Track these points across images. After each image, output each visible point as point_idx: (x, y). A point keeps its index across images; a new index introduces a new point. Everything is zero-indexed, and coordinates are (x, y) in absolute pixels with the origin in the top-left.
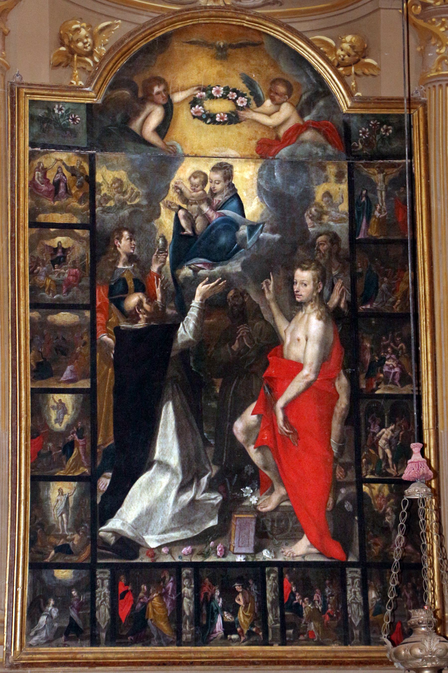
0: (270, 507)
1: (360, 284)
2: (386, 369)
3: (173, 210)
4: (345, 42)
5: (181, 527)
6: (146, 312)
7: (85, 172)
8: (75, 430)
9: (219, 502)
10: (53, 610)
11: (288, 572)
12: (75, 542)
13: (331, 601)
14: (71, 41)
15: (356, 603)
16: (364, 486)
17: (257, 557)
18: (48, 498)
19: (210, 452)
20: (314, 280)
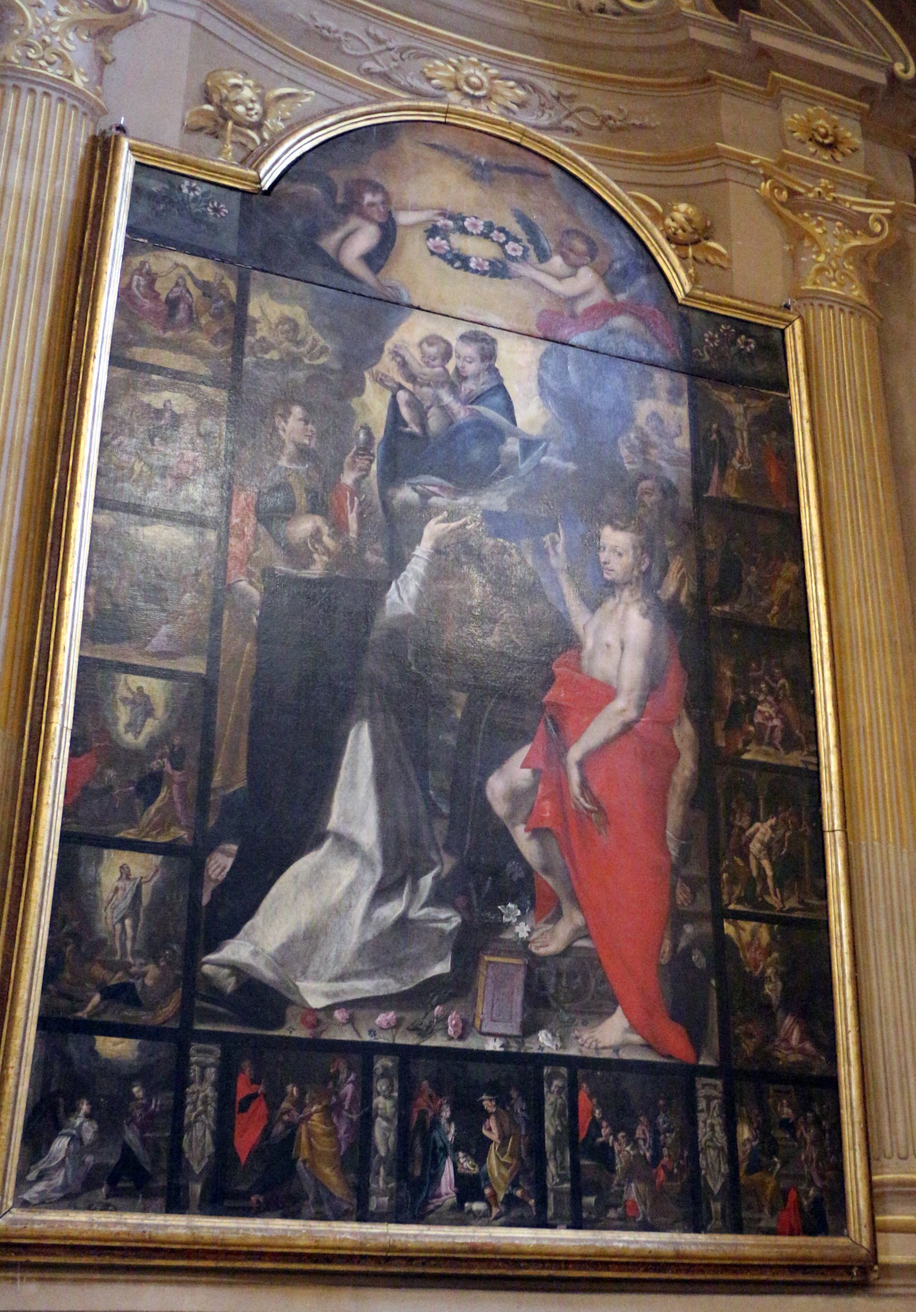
0: (554, 946)
1: (713, 571)
2: (758, 719)
3: (387, 387)
4: (678, 211)
5: (377, 970)
6: (327, 552)
7: (229, 294)
8: (168, 751)
9: (454, 929)
10: (86, 1124)
11: (587, 1078)
12: (149, 982)
13: (669, 1141)
14: (225, 100)
15: (715, 1148)
16: (725, 924)
17: (527, 1045)
18: (96, 883)
19: (441, 828)
20: (634, 548)
